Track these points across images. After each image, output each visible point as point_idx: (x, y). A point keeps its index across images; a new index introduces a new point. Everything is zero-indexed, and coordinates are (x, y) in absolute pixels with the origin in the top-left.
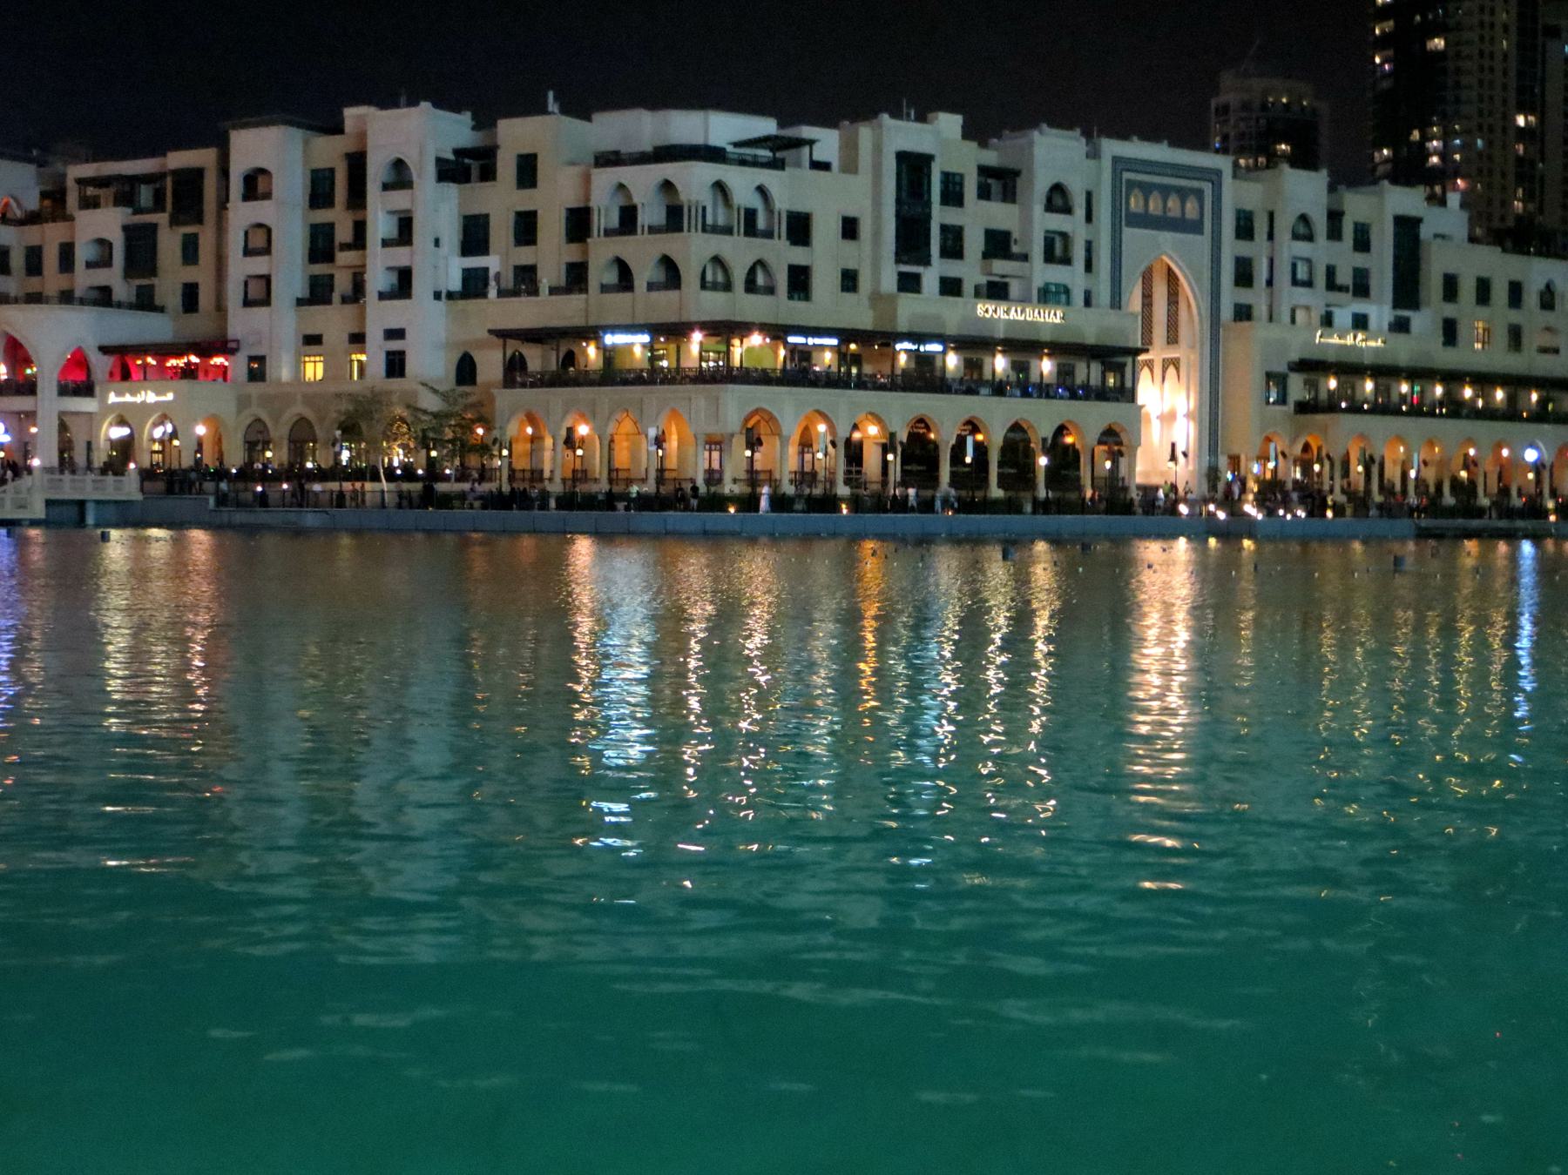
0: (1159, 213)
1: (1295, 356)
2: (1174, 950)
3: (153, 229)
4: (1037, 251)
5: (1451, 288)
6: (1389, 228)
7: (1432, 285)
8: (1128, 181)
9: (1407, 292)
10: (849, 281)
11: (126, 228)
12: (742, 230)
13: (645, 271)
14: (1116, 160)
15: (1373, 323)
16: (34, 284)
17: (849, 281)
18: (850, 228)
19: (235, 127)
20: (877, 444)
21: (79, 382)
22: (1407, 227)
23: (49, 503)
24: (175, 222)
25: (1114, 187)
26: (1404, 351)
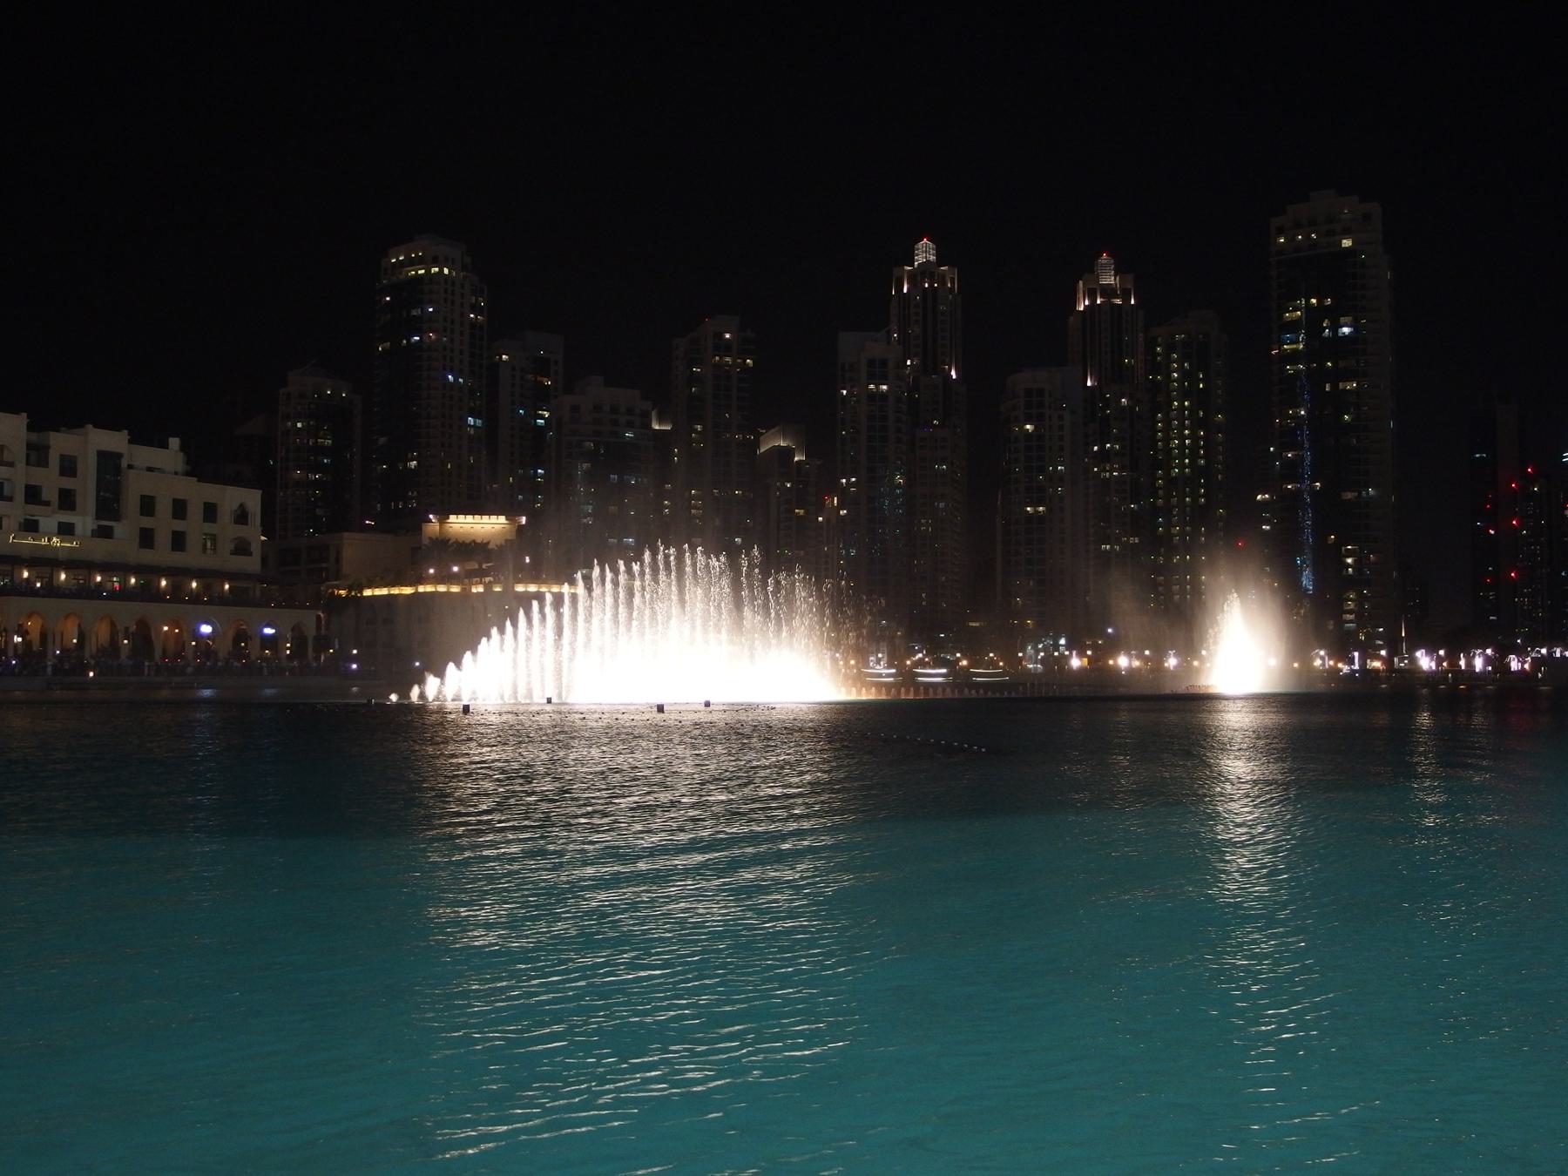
2: (631, 1082)
4: (20, 496)
5: (148, 506)
6: (92, 460)
7: (131, 503)
9: (108, 507)
15: (78, 530)
20: (475, 661)
22: (109, 463)
26: (100, 550)
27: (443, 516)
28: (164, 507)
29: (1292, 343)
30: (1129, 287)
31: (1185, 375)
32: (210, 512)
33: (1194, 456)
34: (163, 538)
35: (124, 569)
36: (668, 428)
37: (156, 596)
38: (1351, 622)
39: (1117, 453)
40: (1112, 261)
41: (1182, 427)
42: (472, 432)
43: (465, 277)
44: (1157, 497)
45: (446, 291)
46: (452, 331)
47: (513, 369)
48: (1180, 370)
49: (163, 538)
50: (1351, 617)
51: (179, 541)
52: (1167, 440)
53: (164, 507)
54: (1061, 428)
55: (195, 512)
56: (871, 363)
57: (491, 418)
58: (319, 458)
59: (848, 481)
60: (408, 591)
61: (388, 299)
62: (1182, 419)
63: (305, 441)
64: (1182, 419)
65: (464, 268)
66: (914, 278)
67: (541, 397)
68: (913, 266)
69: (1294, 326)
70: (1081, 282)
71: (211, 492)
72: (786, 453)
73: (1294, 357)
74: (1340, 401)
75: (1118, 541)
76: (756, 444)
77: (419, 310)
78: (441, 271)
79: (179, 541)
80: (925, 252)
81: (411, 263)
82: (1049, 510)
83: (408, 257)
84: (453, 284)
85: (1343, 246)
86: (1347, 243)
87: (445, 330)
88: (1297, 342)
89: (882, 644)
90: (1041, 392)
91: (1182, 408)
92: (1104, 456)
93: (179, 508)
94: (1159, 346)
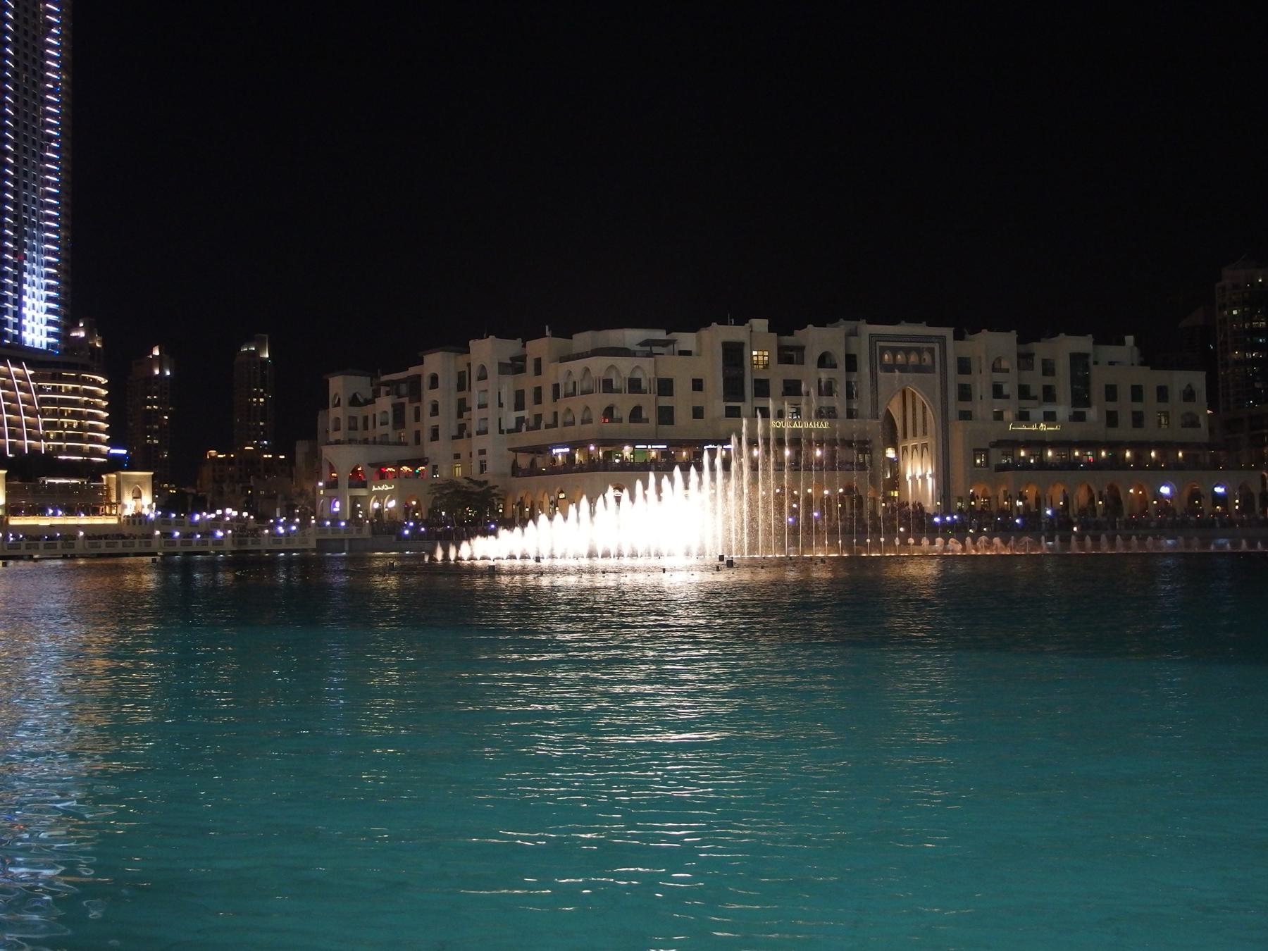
0: (917, 362)
1: (994, 439)
3: (403, 405)
7: (1097, 391)
8: (881, 347)
9: (1081, 398)
10: (698, 413)
11: (393, 405)
12: (601, 390)
13: (649, 413)
14: (871, 336)
16: (353, 434)
17: (698, 413)
18: (698, 385)
19: (425, 354)
21: (358, 481)
22: (1079, 361)
23: (318, 541)
24: (410, 402)
25: (871, 353)
26: (1076, 431)
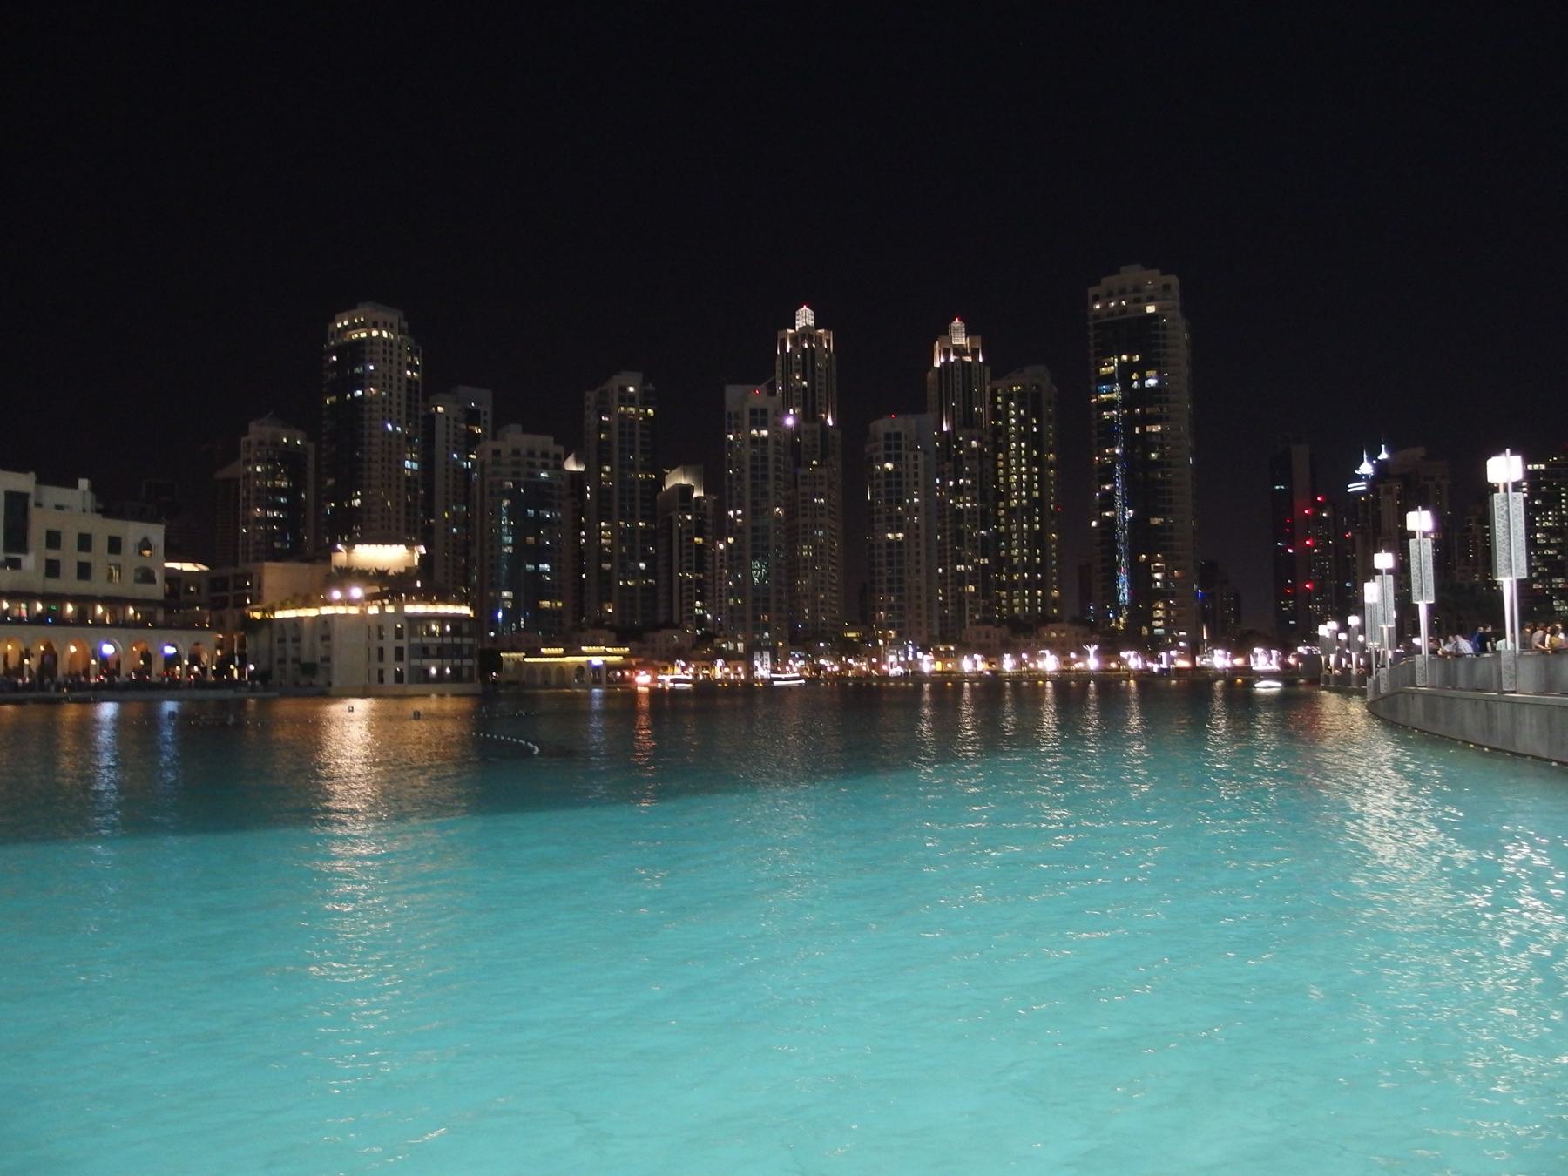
5: (53, 539)
7: (36, 535)
27: (350, 545)
28: (70, 541)
29: (1107, 393)
30: (977, 347)
31: (1021, 420)
32: (115, 545)
33: (1030, 489)
34: (69, 568)
35: (30, 597)
36: (582, 469)
37: (60, 621)
38: (1160, 627)
39: (969, 488)
40: (963, 325)
41: (1019, 465)
42: (409, 474)
43: (402, 340)
44: (999, 525)
45: (385, 352)
46: (391, 386)
47: (448, 419)
48: (1018, 416)
49: (69, 568)
50: (1160, 623)
51: (84, 571)
52: (1007, 475)
53: (70, 541)
54: (916, 466)
55: (101, 544)
56: (753, 412)
57: (427, 462)
58: (277, 498)
59: (735, 513)
60: (312, 612)
61: (334, 358)
62: (1019, 457)
63: (264, 483)
64: (1019, 457)
65: (401, 331)
66: (795, 340)
67: (471, 442)
68: (794, 329)
69: (1109, 379)
70: (937, 343)
71: (115, 527)
72: (687, 490)
73: (1110, 405)
74: (1147, 442)
75: (971, 562)
76: (661, 482)
77: (362, 369)
78: (381, 334)
79: (84, 571)
80: (805, 317)
81: (354, 327)
82: (907, 536)
83: (351, 322)
84: (391, 345)
85: (1148, 311)
86: (1151, 309)
87: (384, 385)
88: (1112, 392)
89: (764, 652)
90: (898, 436)
91: (1019, 448)
92: (958, 490)
93: (85, 542)
94: (999, 396)
